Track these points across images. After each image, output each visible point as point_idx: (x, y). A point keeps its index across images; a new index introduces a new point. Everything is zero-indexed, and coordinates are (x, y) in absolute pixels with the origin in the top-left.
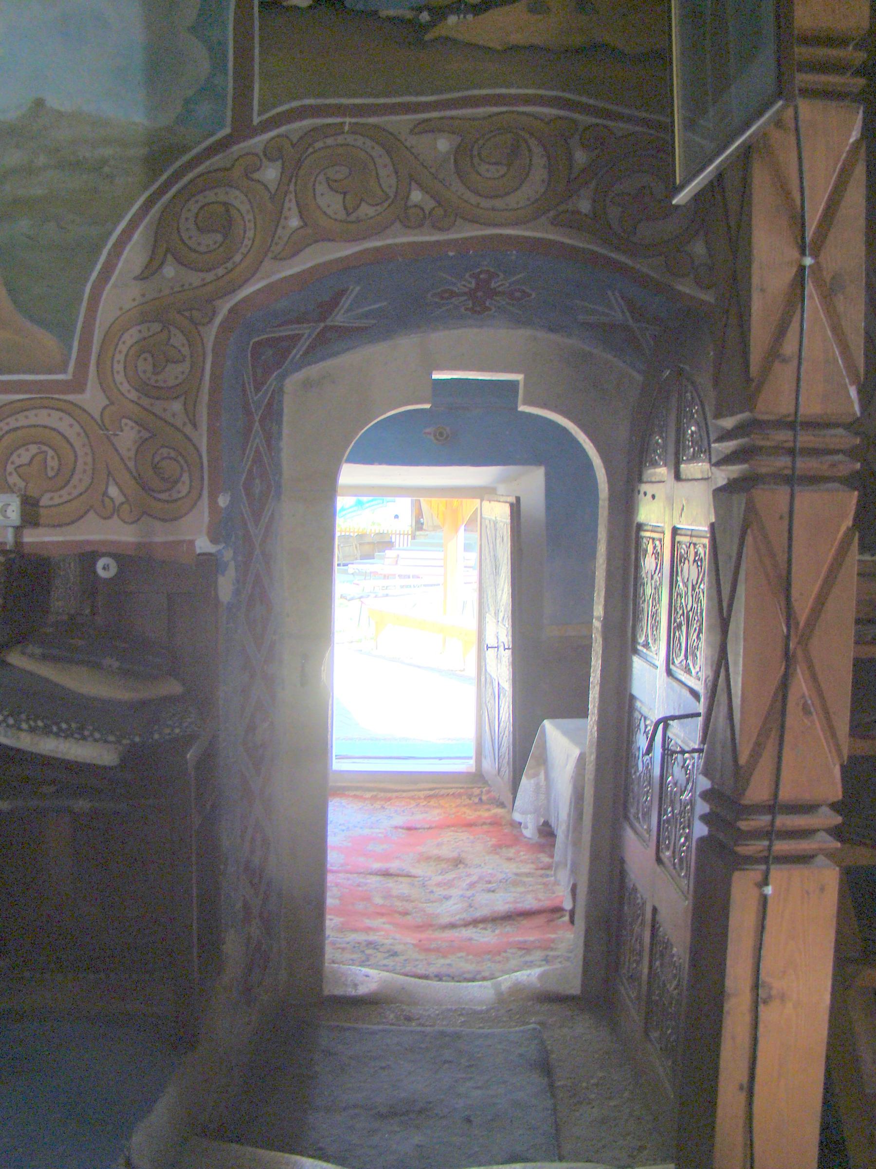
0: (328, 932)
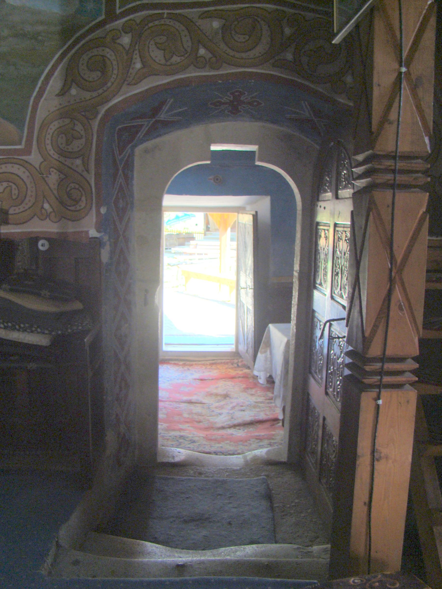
0: (160, 431)
